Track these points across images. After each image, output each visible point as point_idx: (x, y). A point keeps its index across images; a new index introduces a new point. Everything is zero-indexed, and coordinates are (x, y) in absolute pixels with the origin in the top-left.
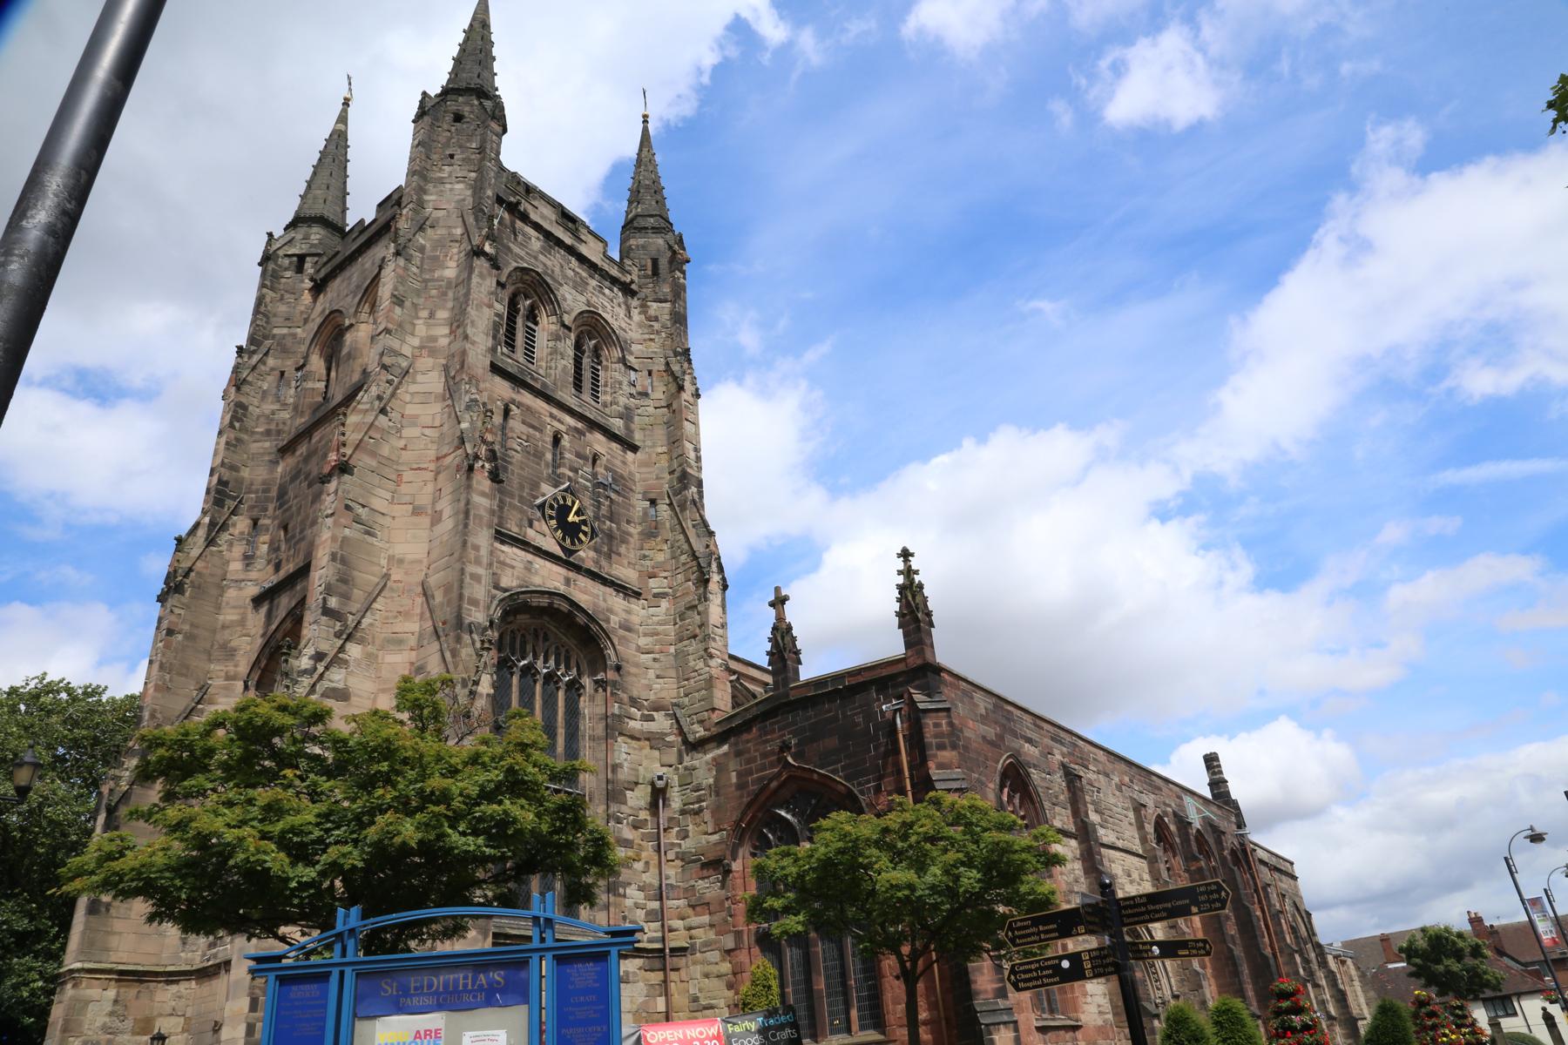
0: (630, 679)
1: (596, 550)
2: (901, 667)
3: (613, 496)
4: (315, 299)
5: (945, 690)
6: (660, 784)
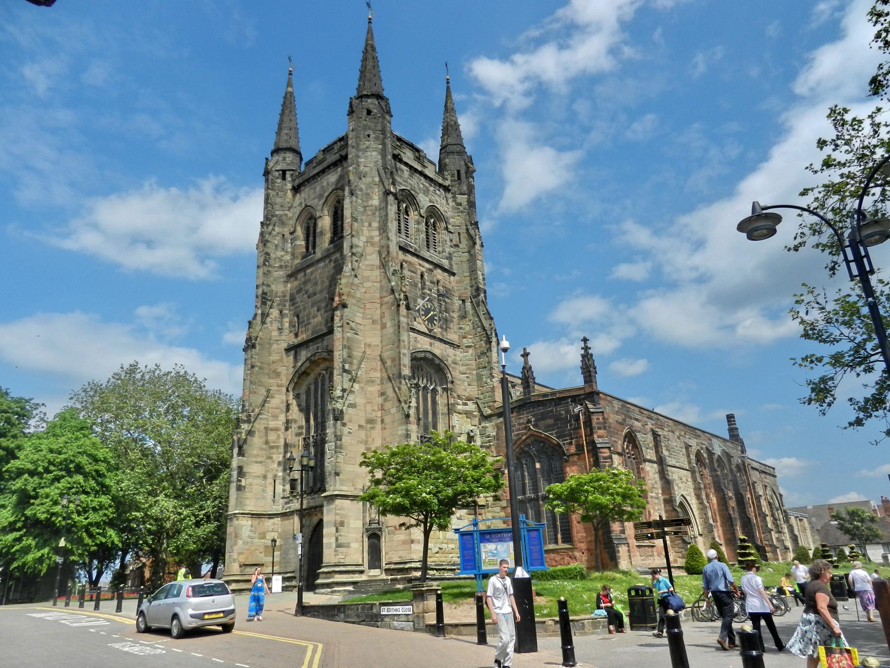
0: (457, 386)
1: (441, 328)
2: (582, 392)
3: (446, 300)
4: (294, 196)
5: (601, 402)
6: (472, 434)
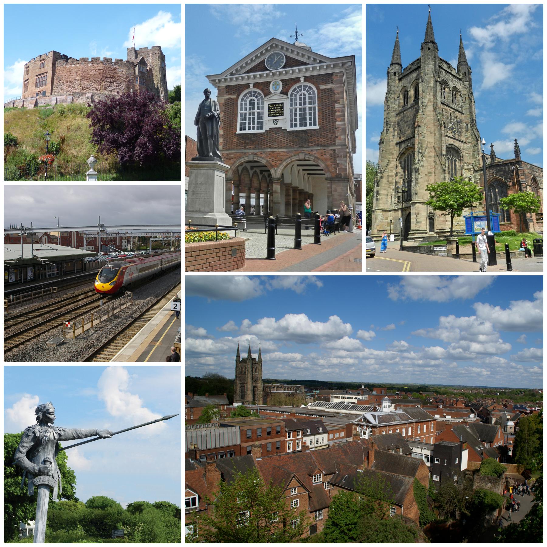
4: (399, 82)
